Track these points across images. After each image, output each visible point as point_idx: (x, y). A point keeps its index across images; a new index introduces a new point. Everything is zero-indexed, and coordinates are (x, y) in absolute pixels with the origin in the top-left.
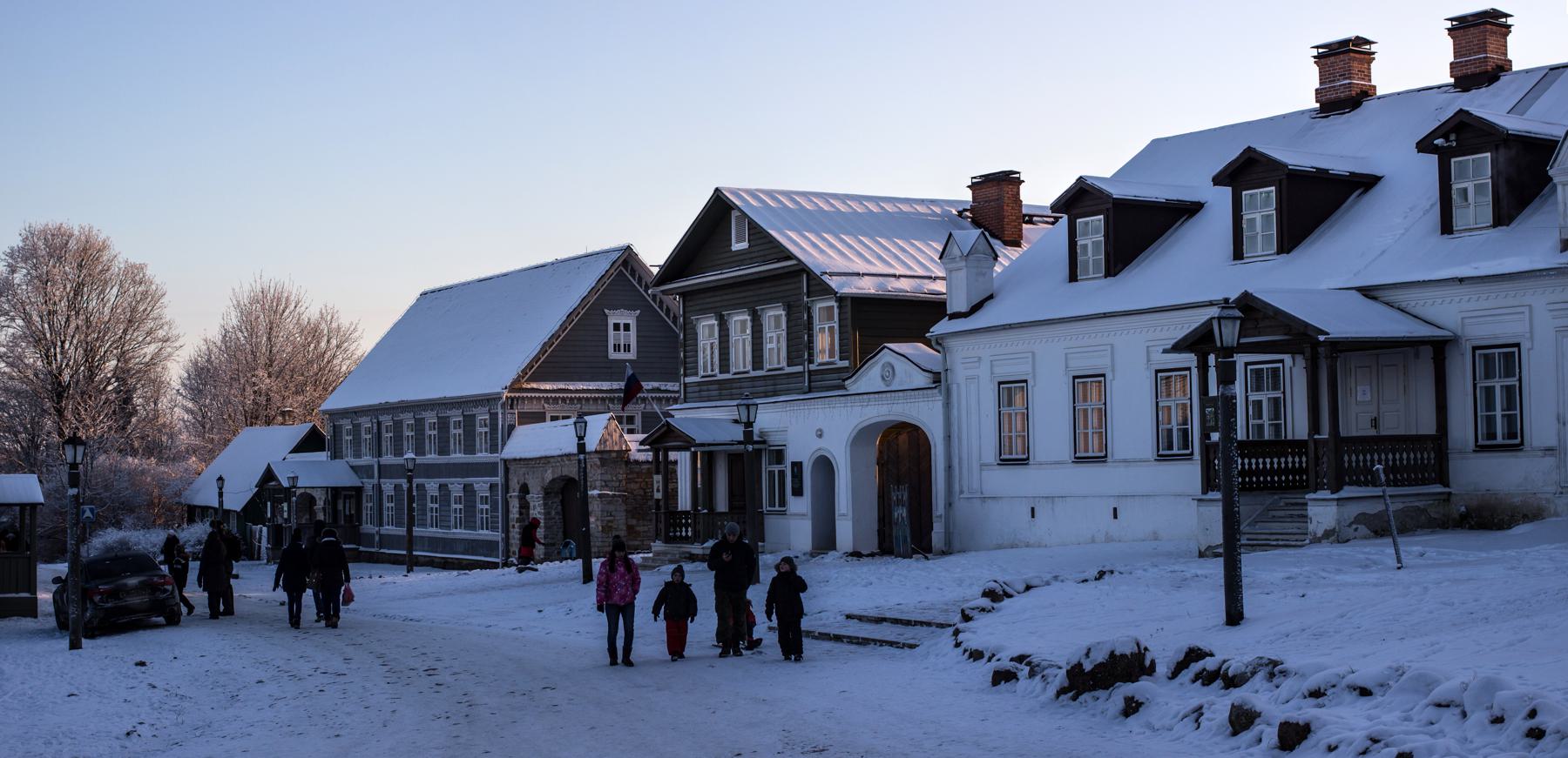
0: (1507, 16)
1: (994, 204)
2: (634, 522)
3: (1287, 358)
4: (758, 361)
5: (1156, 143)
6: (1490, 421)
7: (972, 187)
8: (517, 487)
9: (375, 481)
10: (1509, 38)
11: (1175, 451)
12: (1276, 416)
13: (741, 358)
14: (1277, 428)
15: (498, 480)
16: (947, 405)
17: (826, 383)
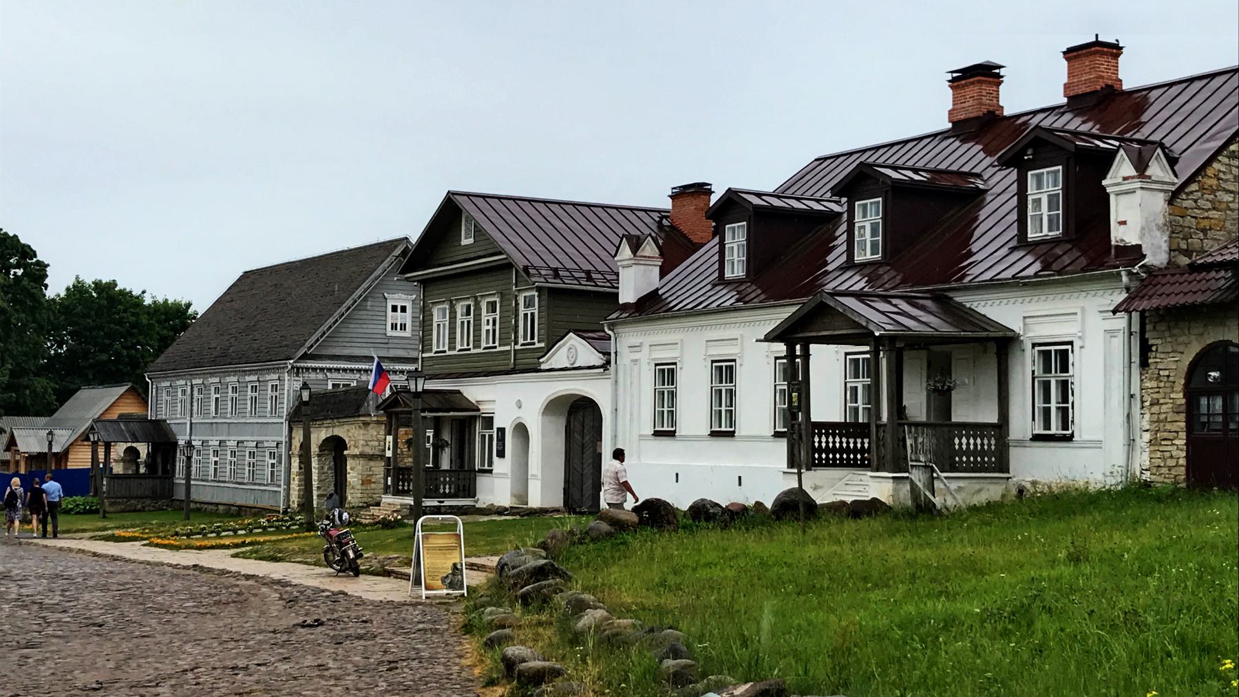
0: (1000, 67)
7: (673, 197)
9: (188, 438)
10: (1065, 80)
15: (284, 439)
17: (525, 365)
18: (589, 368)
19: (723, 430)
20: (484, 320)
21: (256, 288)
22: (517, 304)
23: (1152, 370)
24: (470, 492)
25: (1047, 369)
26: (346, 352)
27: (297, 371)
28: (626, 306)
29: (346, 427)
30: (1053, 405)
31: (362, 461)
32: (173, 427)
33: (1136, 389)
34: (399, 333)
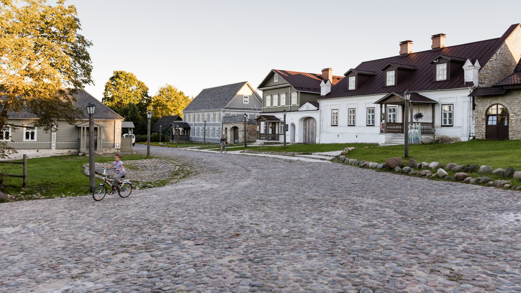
1: (181, 93)
3: (397, 106)
4: (279, 104)
5: (363, 63)
6: (351, 121)
7: (322, 71)
12: (373, 118)
13: (275, 104)
14: (394, 120)
15: (221, 127)
16: (320, 114)
19: (352, 124)
21: (205, 93)
23: (476, 110)
25: (370, 113)
30: (447, 118)
33: (471, 115)
34: (246, 103)
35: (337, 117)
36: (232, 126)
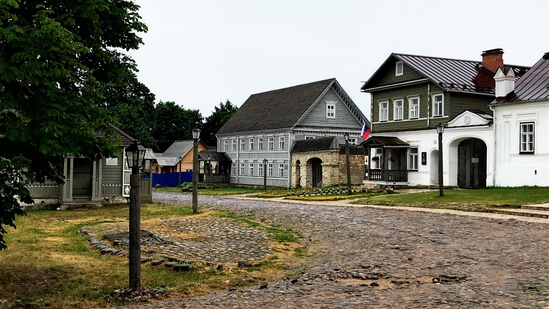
2: (341, 174)
6: (525, 145)
8: (295, 162)
11: (527, 151)
12: (531, 140)
15: (289, 159)
17: (439, 125)
18: (462, 127)
20: (410, 107)
22: (431, 100)
24: (406, 180)
25: (525, 131)
26: (312, 124)
27: (294, 132)
28: (500, 99)
29: (321, 154)
31: (330, 168)
32: (229, 155)
34: (330, 117)
35: (531, 137)
36: (309, 157)
